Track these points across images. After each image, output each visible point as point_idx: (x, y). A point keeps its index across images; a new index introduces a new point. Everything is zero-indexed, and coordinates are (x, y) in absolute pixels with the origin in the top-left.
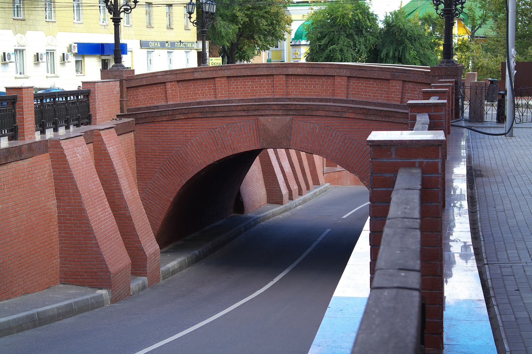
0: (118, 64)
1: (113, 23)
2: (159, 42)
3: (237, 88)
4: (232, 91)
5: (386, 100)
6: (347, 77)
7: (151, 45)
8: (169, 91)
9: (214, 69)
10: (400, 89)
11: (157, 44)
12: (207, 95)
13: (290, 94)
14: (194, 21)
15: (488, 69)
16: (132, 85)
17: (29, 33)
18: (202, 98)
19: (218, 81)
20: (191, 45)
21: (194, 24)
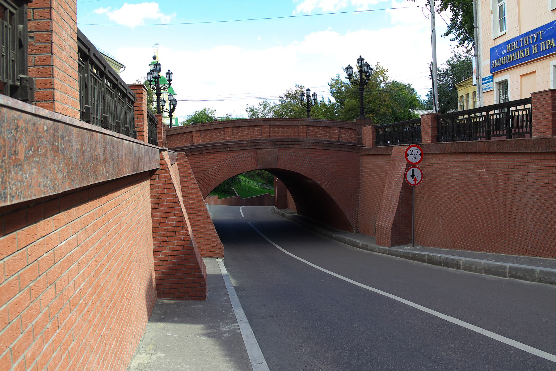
1: (157, 97)
4: (235, 136)
5: (329, 139)
6: (306, 126)
8: (194, 137)
10: (338, 133)
13: (272, 137)
16: (170, 134)
18: (216, 140)
19: (227, 130)
21: (166, 87)
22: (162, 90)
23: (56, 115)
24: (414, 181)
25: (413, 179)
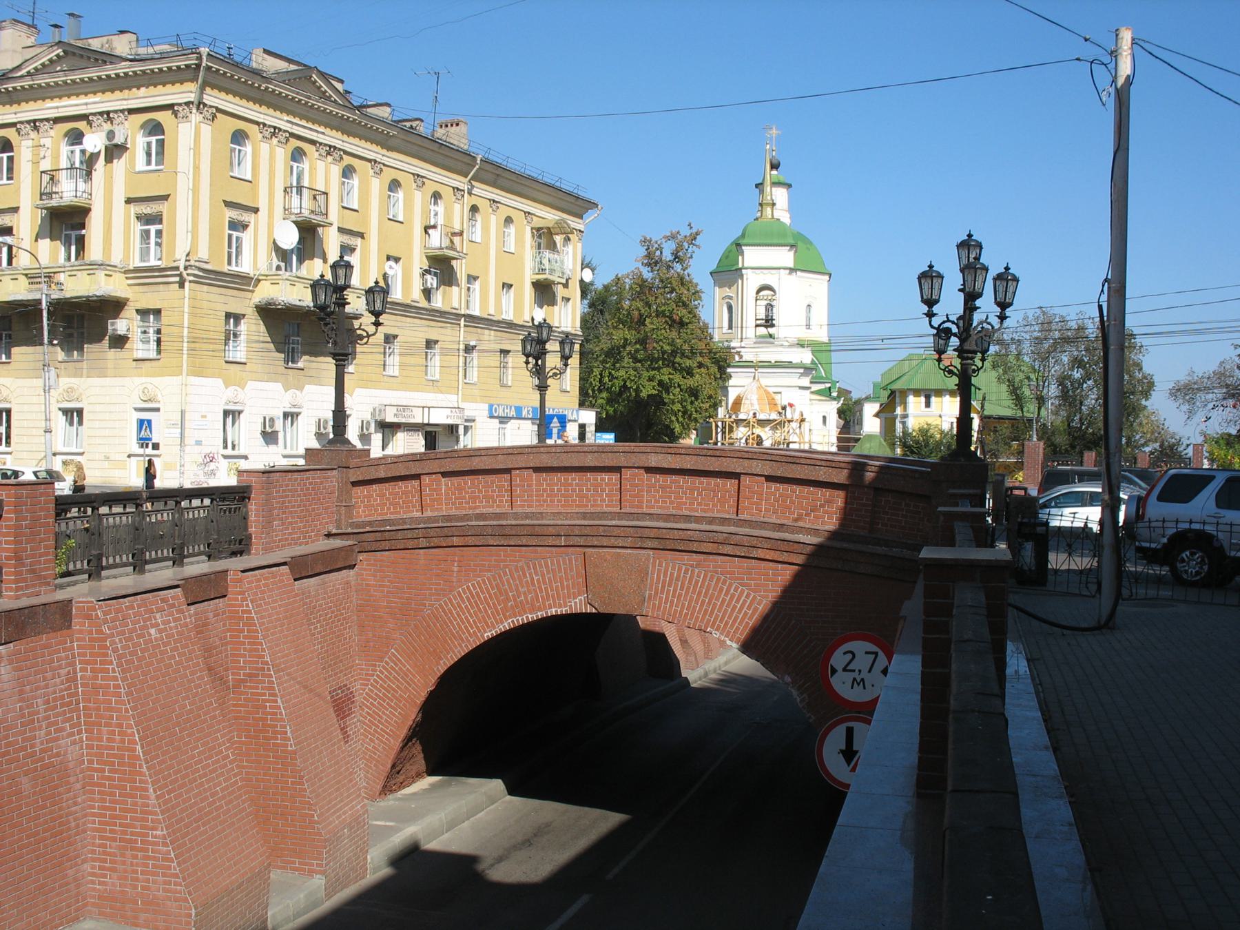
0: (339, 438)
2: (513, 408)
3: (552, 490)
9: (510, 451)
14: (940, 325)
19: (517, 475)
21: (365, 334)
22: (550, 377)
24: (857, 752)
25: (849, 765)
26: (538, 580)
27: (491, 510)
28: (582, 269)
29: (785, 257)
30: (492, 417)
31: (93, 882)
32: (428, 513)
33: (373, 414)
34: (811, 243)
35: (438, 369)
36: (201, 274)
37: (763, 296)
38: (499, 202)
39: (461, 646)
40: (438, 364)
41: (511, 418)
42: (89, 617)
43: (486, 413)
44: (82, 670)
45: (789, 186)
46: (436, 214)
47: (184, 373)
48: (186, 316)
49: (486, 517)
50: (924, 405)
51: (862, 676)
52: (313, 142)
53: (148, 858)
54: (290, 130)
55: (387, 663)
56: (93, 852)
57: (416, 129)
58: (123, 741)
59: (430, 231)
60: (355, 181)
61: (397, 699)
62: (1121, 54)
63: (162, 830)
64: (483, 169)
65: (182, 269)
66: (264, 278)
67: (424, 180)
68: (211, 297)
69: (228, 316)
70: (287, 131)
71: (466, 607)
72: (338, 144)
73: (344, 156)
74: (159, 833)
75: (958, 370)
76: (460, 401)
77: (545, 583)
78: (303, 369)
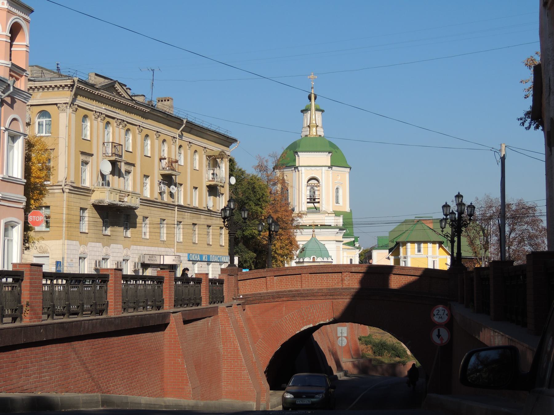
2: (199, 255)
4: (257, 284)
7: (191, 258)
11: (197, 257)
12: (295, 286)
15: (404, 351)
17: (112, 246)
20: (225, 259)
23: (111, 278)
24: (441, 335)
25: (439, 339)
26: (315, 312)
27: (293, 289)
28: (230, 178)
29: (325, 158)
30: (189, 261)
31: (224, 388)
32: (269, 291)
33: (139, 259)
34: (338, 148)
35: (165, 235)
36: (72, 189)
37: (312, 184)
38: (207, 148)
39: (286, 336)
40: (165, 232)
41: (197, 261)
42: (223, 311)
43: (186, 259)
44: (221, 327)
45: (322, 111)
46: (163, 151)
47: (64, 239)
48: (65, 209)
49: (292, 291)
50: (416, 250)
51: (441, 316)
52: (114, 118)
53: (242, 379)
54: (106, 114)
55: (258, 344)
56: (224, 379)
57: (154, 107)
58: (234, 346)
59: (162, 161)
60: (110, 129)
61: (262, 357)
62: (502, 151)
63: (247, 371)
64: (187, 126)
65: (63, 185)
66: (97, 189)
67: (160, 134)
68: (75, 200)
69: (81, 209)
70: (104, 114)
71: (288, 322)
72: (104, 112)
73: (127, 124)
74: (246, 372)
75: (450, 235)
76: (175, 252)
77: (318, 312)
78: (110, 236)
